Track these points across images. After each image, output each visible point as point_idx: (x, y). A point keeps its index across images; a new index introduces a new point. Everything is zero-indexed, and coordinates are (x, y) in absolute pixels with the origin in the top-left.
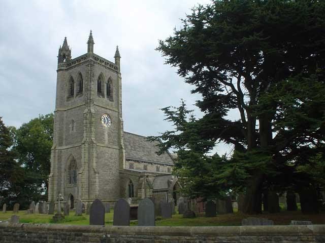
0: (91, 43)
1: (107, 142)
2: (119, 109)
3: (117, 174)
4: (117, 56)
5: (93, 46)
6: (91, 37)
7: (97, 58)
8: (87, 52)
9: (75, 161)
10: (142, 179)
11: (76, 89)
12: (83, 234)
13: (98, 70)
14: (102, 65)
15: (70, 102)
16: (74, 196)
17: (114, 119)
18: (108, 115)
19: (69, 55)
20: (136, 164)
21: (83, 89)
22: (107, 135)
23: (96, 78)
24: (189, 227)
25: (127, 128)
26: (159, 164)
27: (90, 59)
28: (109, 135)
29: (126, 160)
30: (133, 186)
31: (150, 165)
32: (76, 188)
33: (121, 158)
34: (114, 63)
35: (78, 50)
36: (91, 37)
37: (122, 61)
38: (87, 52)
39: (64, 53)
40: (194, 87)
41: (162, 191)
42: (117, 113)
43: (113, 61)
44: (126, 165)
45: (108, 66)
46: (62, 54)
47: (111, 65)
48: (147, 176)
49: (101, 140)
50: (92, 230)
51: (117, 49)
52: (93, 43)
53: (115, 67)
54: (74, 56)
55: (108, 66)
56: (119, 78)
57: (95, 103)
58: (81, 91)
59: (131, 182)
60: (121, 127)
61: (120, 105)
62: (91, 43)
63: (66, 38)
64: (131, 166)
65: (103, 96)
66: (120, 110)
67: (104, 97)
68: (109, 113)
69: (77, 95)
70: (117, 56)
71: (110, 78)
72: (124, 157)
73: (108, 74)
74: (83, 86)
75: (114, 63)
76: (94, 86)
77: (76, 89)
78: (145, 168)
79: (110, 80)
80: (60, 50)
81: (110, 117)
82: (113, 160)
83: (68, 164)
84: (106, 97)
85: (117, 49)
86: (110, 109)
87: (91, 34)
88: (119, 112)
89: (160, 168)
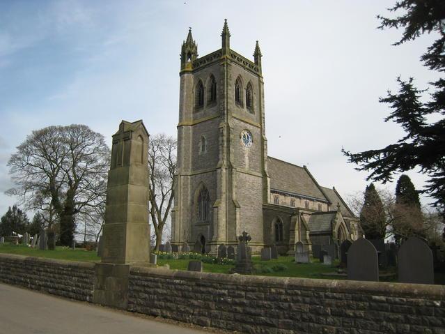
0: (225, 35)
1: (247, 166)
2: (261, 125)
3: (261, 210)
4: (257, 54)
5: (229, 40)
6: (226, 28)
7: (234, 55)
8: (221, 47)
9: (206, 190)
10: (294, 217)
11: (207, 95)
12: (374, 297)
13: (235, 71)
14: (241, 65)
15: (198, 114)
16: (205, 236)
17: (255, 137)
18: (249, 131)
19: (196, 54)
20: (281, 198)
21: (217, 97)
22: (247, 158)
23: (233, 82)
24: (282, 278)
25: (272, 151)
26: (308, 199)
27: (223, 57)
28: (250, 159)
29: (272, 192)
30: (281, 225)
31: (298, 199)
32: (209, 227)
33: (265, 189)
34: (254, 62)
35: (207, 46)
36: (226, 28)
37: (263, 61)
38: (221, 47)
39: (188, 49)
40: (392, 104)
41: (322, 235)
42: (259, 130)
43: (252, 60)
44: (271, 200)
45: (248, 67)
46: (186, 52)
47: (251, 65)
48: (302, 214)
49: (242, 164)
50: (393, 290)
51: (257, 44)
52: (229, 36)
53: (255, 67)
54: (202, 53)
55: (248, 67)
56: (261, 83)
57: (234, 115)
58: (213, 99)
59: (278, 220)
60: (265, 147)
61: (263, 119)
62: (225, 35)
63: (257, 42)
64: (276, 200)
65: (243, 107)
66: (263, 124)
67: (243, 107)
68: (249, 129)
69: (208, 105)
70: (257, 54)
71: (249, 83)
72: (269, 188)
73: (248, 76)
74: (217, 92)
75: (254, 62)
76: (231, 93)
77: (207, 95)
78: (292, 202)
79: (250, 85)
80: (184, 47)
81: (250, 134)
82: (255, 192)
83: (197, 193)
84: (245, 106)
85: (257, 44)
86: (250, 124)
87: (226, 23)
88: (261, 128)
89: (280, 199)
